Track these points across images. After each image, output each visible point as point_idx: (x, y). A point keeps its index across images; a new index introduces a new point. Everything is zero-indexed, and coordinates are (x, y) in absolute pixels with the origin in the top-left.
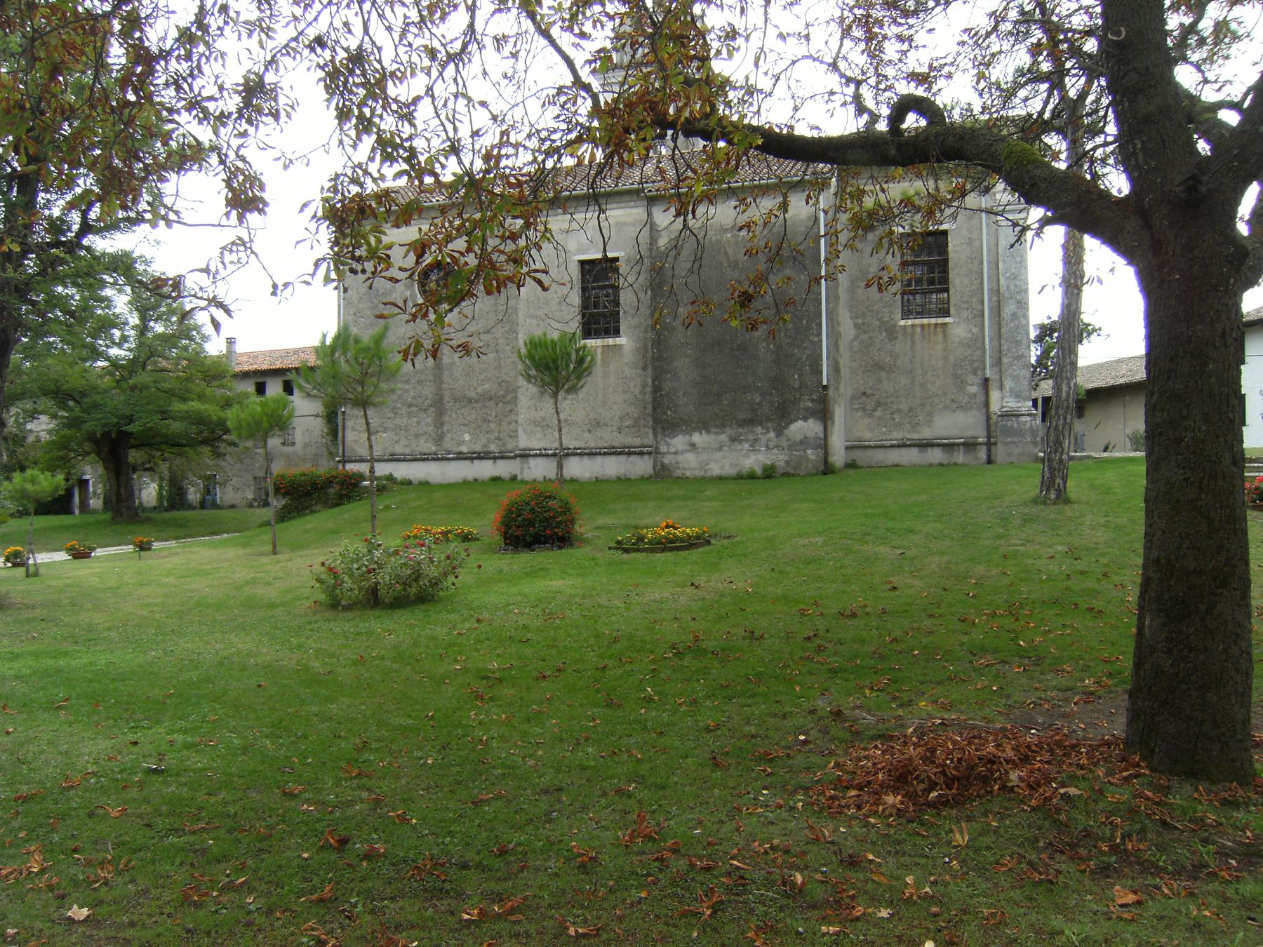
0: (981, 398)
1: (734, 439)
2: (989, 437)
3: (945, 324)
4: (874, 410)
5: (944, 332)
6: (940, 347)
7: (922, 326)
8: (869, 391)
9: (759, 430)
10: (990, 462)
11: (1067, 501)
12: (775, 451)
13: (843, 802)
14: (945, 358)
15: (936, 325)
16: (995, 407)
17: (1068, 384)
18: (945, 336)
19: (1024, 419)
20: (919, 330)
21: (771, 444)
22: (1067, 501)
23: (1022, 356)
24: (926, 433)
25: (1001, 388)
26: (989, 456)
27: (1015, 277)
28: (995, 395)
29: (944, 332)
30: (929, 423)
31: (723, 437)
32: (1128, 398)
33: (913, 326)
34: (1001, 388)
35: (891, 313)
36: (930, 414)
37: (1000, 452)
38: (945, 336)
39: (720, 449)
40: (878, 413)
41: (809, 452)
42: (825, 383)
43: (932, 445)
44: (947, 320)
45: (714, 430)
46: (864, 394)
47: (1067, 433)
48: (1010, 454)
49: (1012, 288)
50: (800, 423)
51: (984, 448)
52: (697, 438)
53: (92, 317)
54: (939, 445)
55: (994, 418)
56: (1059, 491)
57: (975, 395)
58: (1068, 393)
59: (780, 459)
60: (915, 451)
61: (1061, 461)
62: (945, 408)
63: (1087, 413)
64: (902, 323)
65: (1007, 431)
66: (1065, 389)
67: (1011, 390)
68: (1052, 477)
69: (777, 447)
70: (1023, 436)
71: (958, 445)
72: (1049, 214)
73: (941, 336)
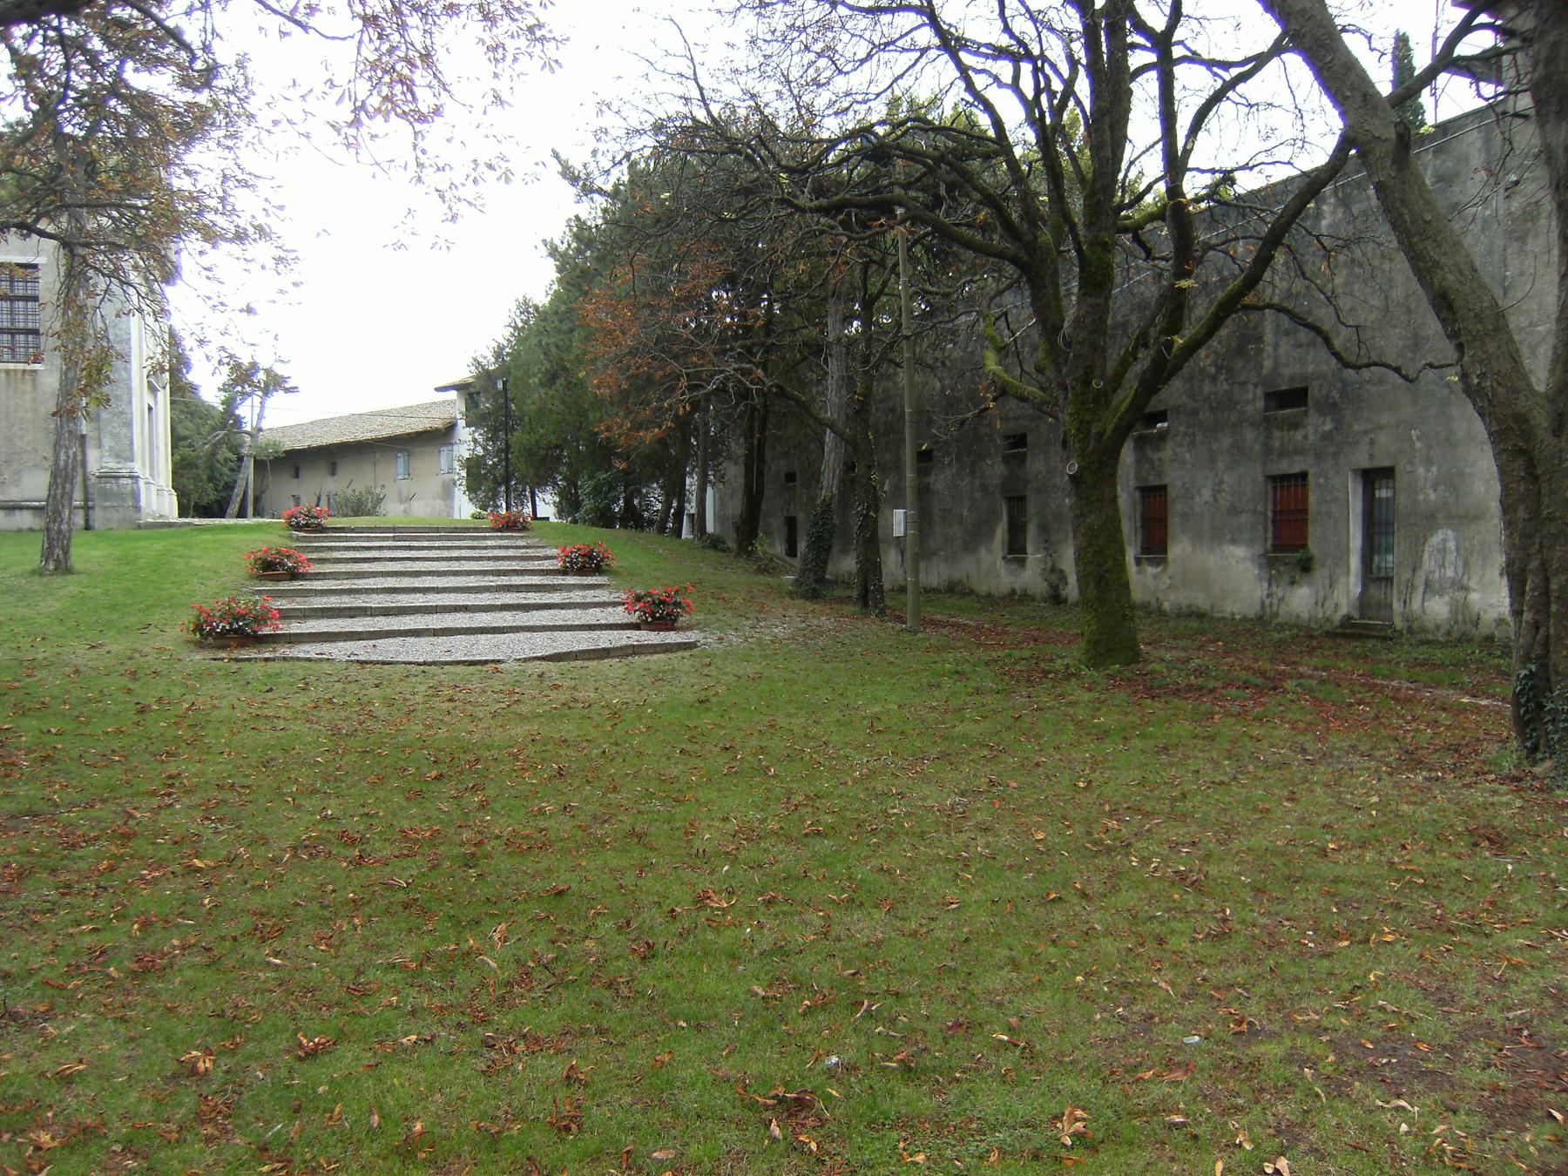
2: (86, 500)
3: (35, 371)
5: (34, 380)
6: (28, 397)
10: (88, 527)
11: (68, 571)
13: (621, 1115)
14: (35, 410)
17: (67, 453)
18: (34, 386)
19: (125, 481)
22: (68, 571)
25: (100, 446)
26: (87, 521)
29: (34, 380)
30: (17, 483)
32: (378, 456)
34: (100, 446)
36: (18, 472)
37: (98, 517)
38: (34, 386)
43: (21, 508)
44: (37, 367)
47: (66, 503)
48: (109, 520)
51: (81, 512)
54: (28, 508)
55: (93, 479)
56: (57, 561)
58: (66, 462)
61: (60, 531)
62: (36, 466)
63: (341, 469)
65: (106, 495)
66: (63, 457)
67: (111, 449)
68: (51, 547)
70: (123, 499)
72: (1128, 25)
73: (29, 385)
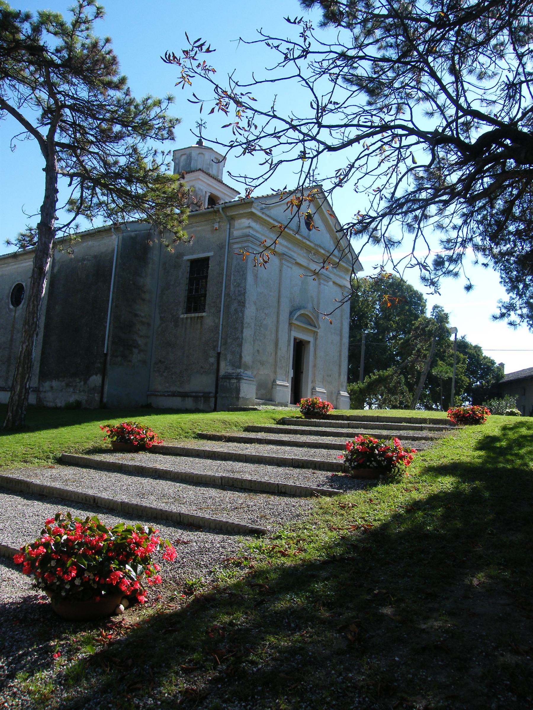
0: (215, 366)
1: (68, 385)
3: (202, 317)
4: (164, 372)
7: (191, 318)
8: (163, 360)
9: (78, 380)
12: (82, 393)
15: (198, 317)
16: (222, 373)
20: (189, 320)
21: (81, 389)
23: (238, 338)
24: (187, 388)
27: (239, 285)
28: (223, 364)
31: (63, 384)
33: (187, 318)
35: (177, 310)
39: (61, 390)
40: (165, 374)
41: (96, 395)
42: (105, 352)
43: (188, 396)
45: (61, 379)
46: (160, 361)
49: (237, 292)
50: (94, 376)
52: (55, 383)
53: (449, 346)
57: (213, 364)
59: (82, 397)
60: (179, 399)
64: (182, 316)
69: (84, 391)
71: (201, 397)
